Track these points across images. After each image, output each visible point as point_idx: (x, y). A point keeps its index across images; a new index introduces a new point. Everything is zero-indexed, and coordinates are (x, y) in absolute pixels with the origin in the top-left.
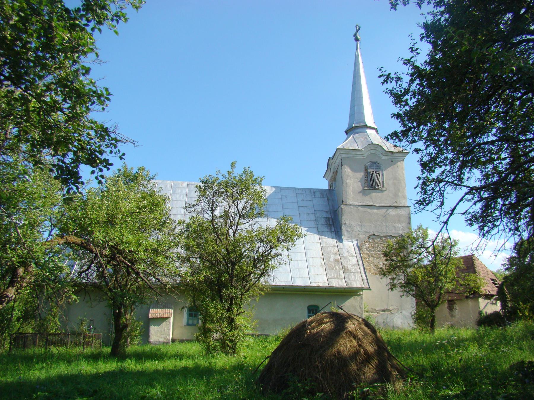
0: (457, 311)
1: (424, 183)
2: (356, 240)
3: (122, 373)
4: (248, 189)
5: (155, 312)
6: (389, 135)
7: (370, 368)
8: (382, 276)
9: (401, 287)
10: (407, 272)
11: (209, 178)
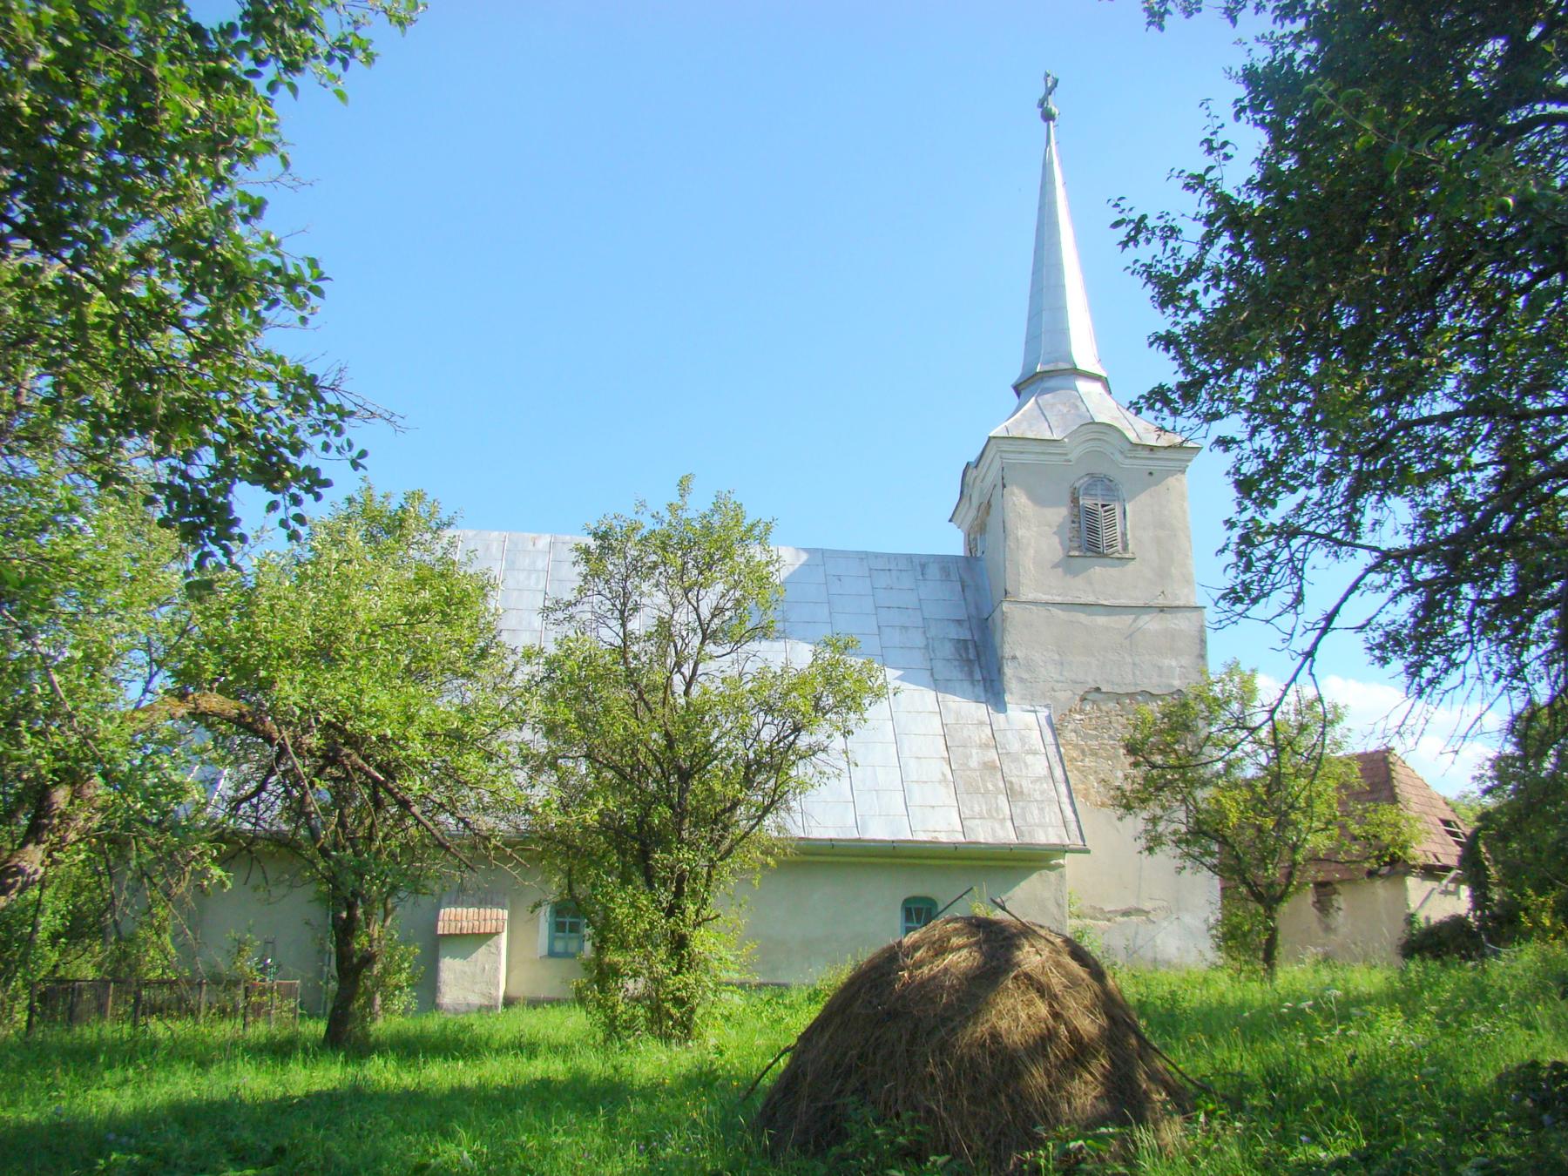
0: (1341, 913)
1: (1245, 539)
2: (1047, 706)
3: (357, 1097)
4: (728, 554)
5: (454, 918)
6: (1141, 397)
7: (1086, 1083)
8: (1120, 811)
9: (1177, 843)
10: (1194, 799)
11: (615, 522)
